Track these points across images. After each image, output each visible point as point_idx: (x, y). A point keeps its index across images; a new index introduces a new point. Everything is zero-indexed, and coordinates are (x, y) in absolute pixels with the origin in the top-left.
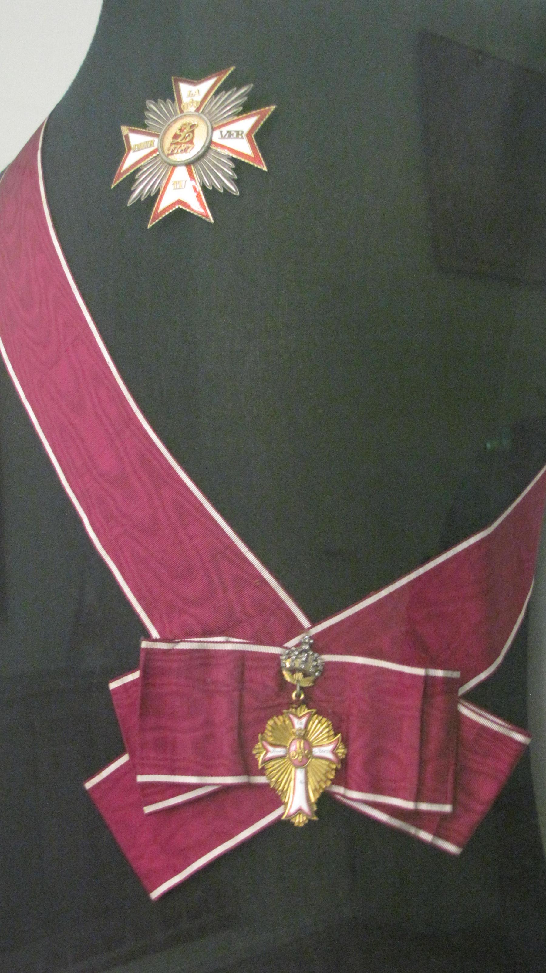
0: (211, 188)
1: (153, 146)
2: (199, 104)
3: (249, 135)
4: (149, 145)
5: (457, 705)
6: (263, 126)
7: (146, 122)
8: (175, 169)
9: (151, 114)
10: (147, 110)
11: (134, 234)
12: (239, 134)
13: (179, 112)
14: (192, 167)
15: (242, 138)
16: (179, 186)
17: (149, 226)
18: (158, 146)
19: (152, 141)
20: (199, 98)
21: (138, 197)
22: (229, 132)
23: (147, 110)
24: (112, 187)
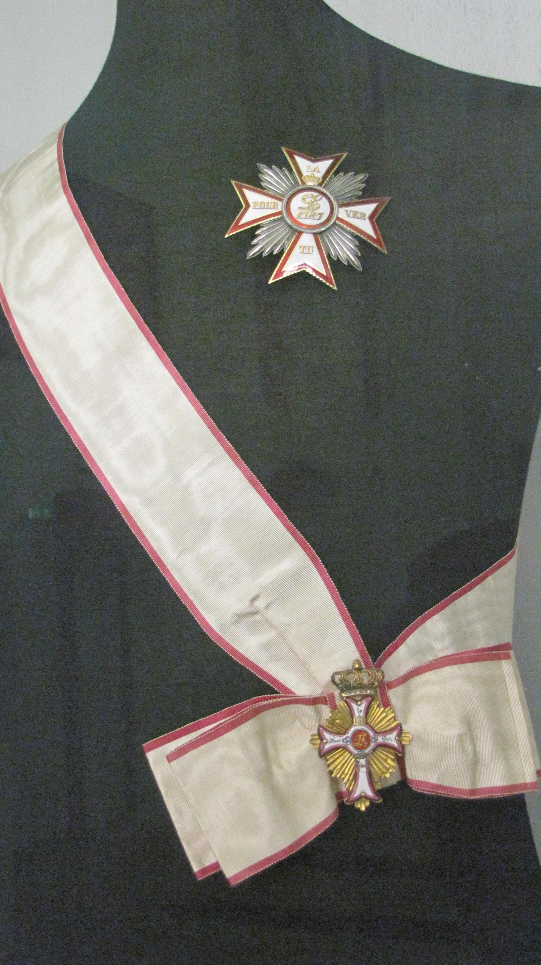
0: (336, 259)
1: (277, 209)
2: (321, 180)
3: (371, 218)
4: (272, 207)
5: (233, 889)
6: (252, 185)
7: (263, 184)
8: (300, 235)
9: (266, 177)
10: (262, 173)
11: (511, 312)
12: (363, 216)
13: (300, 183)
14: (318, 236)
15: (365, 219)
16: (306, 250)
17: (271, 281)
18: (282, 210)
19: (275, 203)
20: (320, 175)
21: (259, 253)
22: (355, 213)
23: (262, 173)
24: (227, 236)
